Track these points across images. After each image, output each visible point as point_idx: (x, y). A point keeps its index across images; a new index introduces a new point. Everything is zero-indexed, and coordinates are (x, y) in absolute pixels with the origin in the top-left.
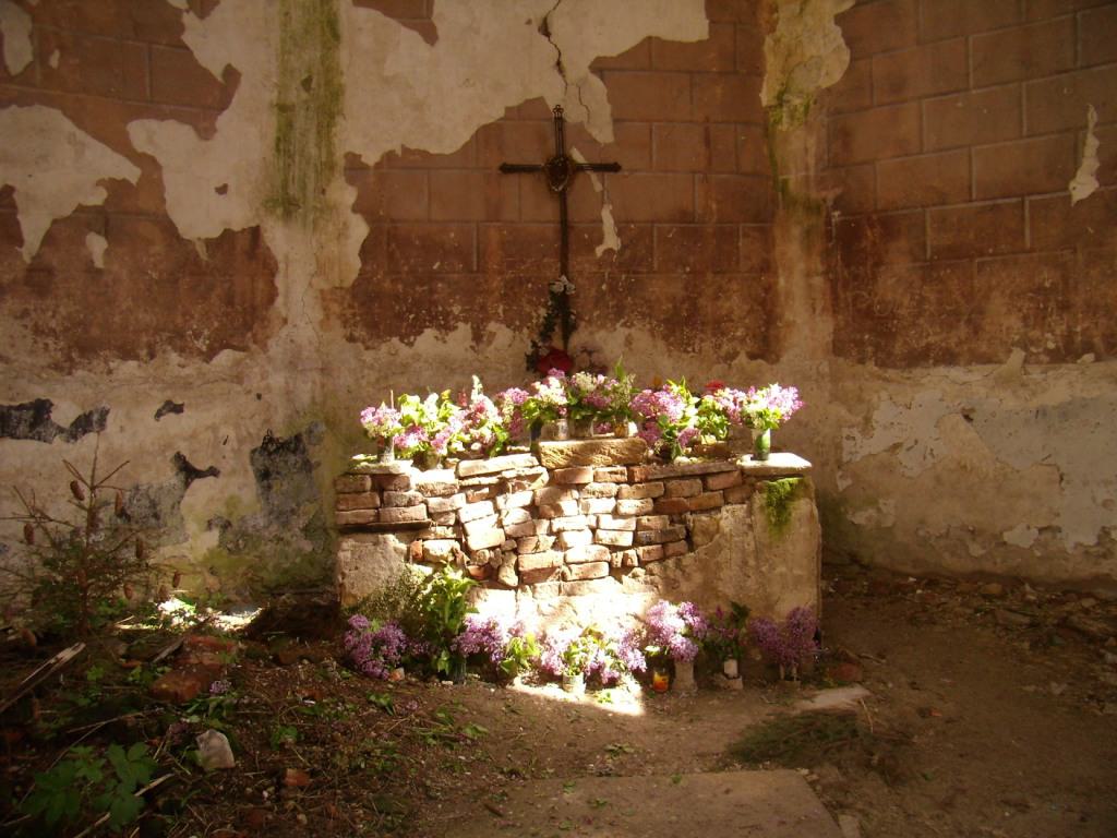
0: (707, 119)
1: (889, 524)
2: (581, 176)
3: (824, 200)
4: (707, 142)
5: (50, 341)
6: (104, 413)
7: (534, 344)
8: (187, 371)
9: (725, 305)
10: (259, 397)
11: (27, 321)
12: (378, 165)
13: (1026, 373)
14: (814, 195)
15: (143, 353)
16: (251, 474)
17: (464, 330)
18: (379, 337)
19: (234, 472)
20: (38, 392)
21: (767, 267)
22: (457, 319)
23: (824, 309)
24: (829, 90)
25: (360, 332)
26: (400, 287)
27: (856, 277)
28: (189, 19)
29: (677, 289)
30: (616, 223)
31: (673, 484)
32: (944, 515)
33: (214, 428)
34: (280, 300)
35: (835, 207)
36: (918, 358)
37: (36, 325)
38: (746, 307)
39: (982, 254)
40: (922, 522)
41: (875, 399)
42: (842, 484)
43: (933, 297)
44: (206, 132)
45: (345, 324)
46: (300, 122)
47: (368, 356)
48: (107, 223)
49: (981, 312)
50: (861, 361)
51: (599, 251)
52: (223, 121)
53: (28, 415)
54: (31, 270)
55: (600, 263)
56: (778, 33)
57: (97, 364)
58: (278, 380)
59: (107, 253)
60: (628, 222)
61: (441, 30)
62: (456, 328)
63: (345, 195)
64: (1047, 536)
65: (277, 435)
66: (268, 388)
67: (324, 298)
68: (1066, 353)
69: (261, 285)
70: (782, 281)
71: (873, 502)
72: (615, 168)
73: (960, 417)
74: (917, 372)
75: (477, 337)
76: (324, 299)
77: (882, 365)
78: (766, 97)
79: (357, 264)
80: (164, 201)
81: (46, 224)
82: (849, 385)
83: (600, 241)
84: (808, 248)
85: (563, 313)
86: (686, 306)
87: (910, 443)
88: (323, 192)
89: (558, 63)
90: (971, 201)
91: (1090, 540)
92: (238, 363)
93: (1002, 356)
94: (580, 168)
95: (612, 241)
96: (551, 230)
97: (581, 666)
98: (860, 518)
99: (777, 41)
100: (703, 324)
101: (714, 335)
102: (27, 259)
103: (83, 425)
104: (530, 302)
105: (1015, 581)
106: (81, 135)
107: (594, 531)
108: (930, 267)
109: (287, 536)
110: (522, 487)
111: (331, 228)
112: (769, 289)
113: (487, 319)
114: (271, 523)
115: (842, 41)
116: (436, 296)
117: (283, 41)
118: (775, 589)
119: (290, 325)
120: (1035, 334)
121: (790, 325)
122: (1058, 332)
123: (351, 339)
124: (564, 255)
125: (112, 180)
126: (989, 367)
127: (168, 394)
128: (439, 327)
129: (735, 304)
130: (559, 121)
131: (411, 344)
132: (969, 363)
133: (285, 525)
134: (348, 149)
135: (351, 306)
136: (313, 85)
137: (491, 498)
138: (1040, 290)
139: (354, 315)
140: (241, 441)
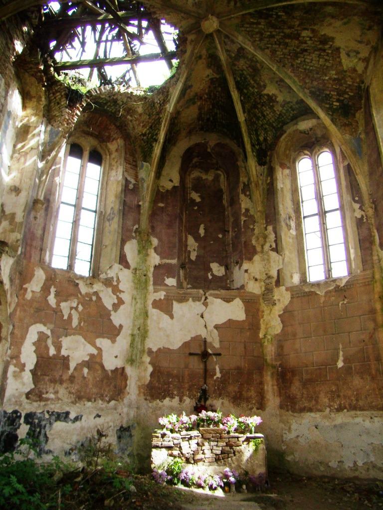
0: (245, 341)
1: (297, 460)
2: (210, 357)
3: (277, 365)
4: (245, 348)
5: (72, 395)
6: (82, 416)
7: (196, 403)
9: (250, 394)
10: (120, 414)
11: (68, 390)
12: (156, 352)
13: (331, 415)
14: (274, 363)
15: (93, 400)
16: (116, 437)
17: (177, 398)
18: (154, 399)
19: (112, 436)
20: (67, 409)
21: (261, 383)
22: (175, 395)
23: (277, 396)
24: (277, 334)
26: (160, 386)
27: (285, 386)
28: (112, 313)
29: (236, 389)
30: (220, 370)
31: (230, 439)
32: (313, 457)
33: (108, 423)
34: (128, 387)
35: (279, 367)
36: (303, 410)
37: (69, 391)
38: (256, 394)
39: (317, 381)
40: (306, 460)
41: (291, 421)
42: (284, 448)
44: (114, 341)
45: (144, 395)
46: (137, 339)
47: (150, 405)
48: (88, 365)
49: (318, 397)
50: (288, 411)
51: (215, 378)
52: (118, 338)
53: (64, 415)
55: (215, 381)
56: (264, 318)
57: (82, 403)
58: (125, 410)
59: (88, 373)
60: (223, 370)
61: (175, 315)
62: (174, 398)
63: (147, 359)
64: (340, 464)
65: (124, 426)
66: (123, 412)
67: (139, 387)
68: (340, 409)
69: (123, 383)
70: (266, 387)
71: (293, 454)
72: (220, 355)
73: (314, 427)
74: (302, 414)
75: (181, 401)
76: (139, 388)
77: (293, 412)
78: (261, 335)
79: (149, 378)
80: (102, 359)
81: (75, 365)
82: (285, 418)
83: (215, 375)
84: (272, 376)
85: (204, 395)
86: (238, 394)
88: (141, 358)
89: (205, 325)
90: (313, 366)
91: (351, 465)
92: (115, 405)
93: (155, 397)
94: (211, 354)
95: (218, 375)
96: (202, 371)
97: (208, 484)
98: (289, 458)
99: (264, 320)
100: (244, 399)
101: (247, 402)
102: (70, 374)
103: (77, 419)
104: (196, 391)
105: (332, 478)
106: (85, 342)
107: (212, 450)
108: (305, 384)
109: (123, 456)
110: (195, 439)
111: (142, 368)
112: (262, 389)
114: (120, 452)
115: (280, 322)
116: (170, 389)
117: (134, 317)
118: (255, 467)
119: (130, 395)
120: (332, 404)
122: (337, 403)
123: (146, 399)
124: (205, 378)
125: (91, 354)
126: (321, 413)
127: (98, 412)
128: (170, 397)
129: (252, 393)
130: (205, 341)
131: (162, 402)
132: (316, 412)
133: (123, 453)
134: (148, 347)
135: (147, 390)
136: (141, 329)
137: (188, 441)
138: (332, 391)
139: (147, 392)
140: (114, 427)
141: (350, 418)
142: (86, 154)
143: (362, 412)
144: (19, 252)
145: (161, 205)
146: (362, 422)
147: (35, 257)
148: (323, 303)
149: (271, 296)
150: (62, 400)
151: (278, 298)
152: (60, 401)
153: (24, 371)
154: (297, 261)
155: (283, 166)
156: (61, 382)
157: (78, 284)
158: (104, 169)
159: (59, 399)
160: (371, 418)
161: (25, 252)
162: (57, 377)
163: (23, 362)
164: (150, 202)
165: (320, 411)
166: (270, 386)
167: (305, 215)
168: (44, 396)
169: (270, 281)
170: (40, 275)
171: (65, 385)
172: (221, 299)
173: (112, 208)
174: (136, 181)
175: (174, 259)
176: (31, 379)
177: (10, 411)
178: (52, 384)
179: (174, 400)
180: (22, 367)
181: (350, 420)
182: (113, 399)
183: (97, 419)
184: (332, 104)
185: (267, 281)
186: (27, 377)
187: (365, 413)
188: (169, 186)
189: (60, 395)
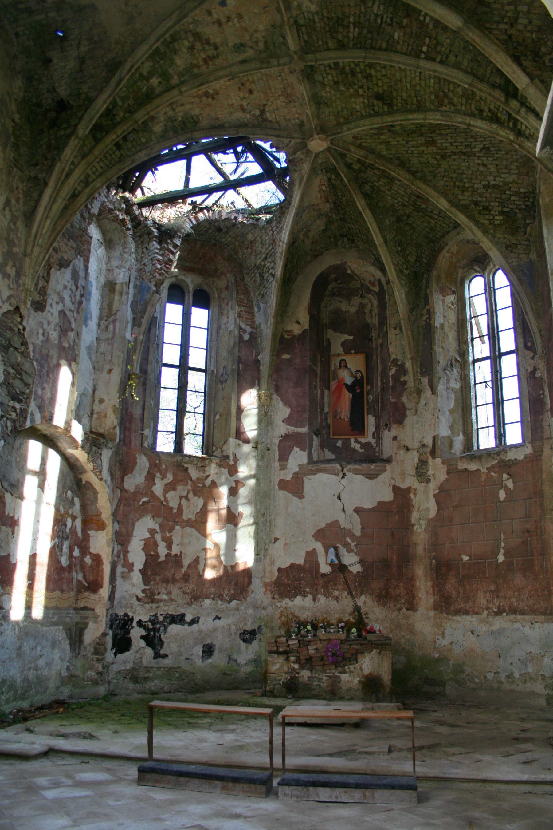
6: (199, 618)
8: (223, 607)
17: (310, 597)
20: (182, 611)
22: (308, 593)
25: (277, 596)
36: (458, 612)
43: (462, 591)
45: (272, 592)
47: (279, 604)
50: (442, 612)
53: (180, 617)
54: (184, 575)
68: (499, 613)
70: (417, 583)
73: (470, 633)
75: (314, 600)
77: (447, 614)
87: (456, 642)
92: (238, 605)
102: (183, 572)
103: (195, 621)
113: (318, 594)
121: (420, 599)
126: (478, 616)
127: (217, 614)
128: (302, 596)
129: (401, 591)
140: (237, 630)
141: (509, 623)
142: (189, 298)
143: (523, 616)
144: (117, 440)
145: (286, 356)
146: (521, 628)
147: (135, 442)
148: (485, 481)
149: (424, 471)
150: (176, 601)
151: (433, 472)
152: (174, 603)
153: (133, 571)
154: (461, 423)
155: (444, 292)
156: (174, 581)
157: (187, 469)
158: (213, 312)
159: (172, 600)
160: (532, 624)
161: (124, 438)
162: (170, 576)
163: (131, 561)
164: (272, 355)
165: (477, 613)
166: (422, 582)
167: (475, 358)
168: (156, 597)
169: (424, 450)
170: (143, 462)
171: (178, 585)
172: (363, 475)
173: (225, 367)
174: (252, 328)
175: (304, 426)
176: (141, 579)
177: (121, 614)
178: (164, 584)
179: (307, 599)
180: (130, 567)
181: (508, 625)
182: (235, 599)
183: (217, 621)
184: (494, 219)
185: (421, 451)
186: (136, 577)
187: (526, 617)
188: (297, 330)
189: (173, 596)
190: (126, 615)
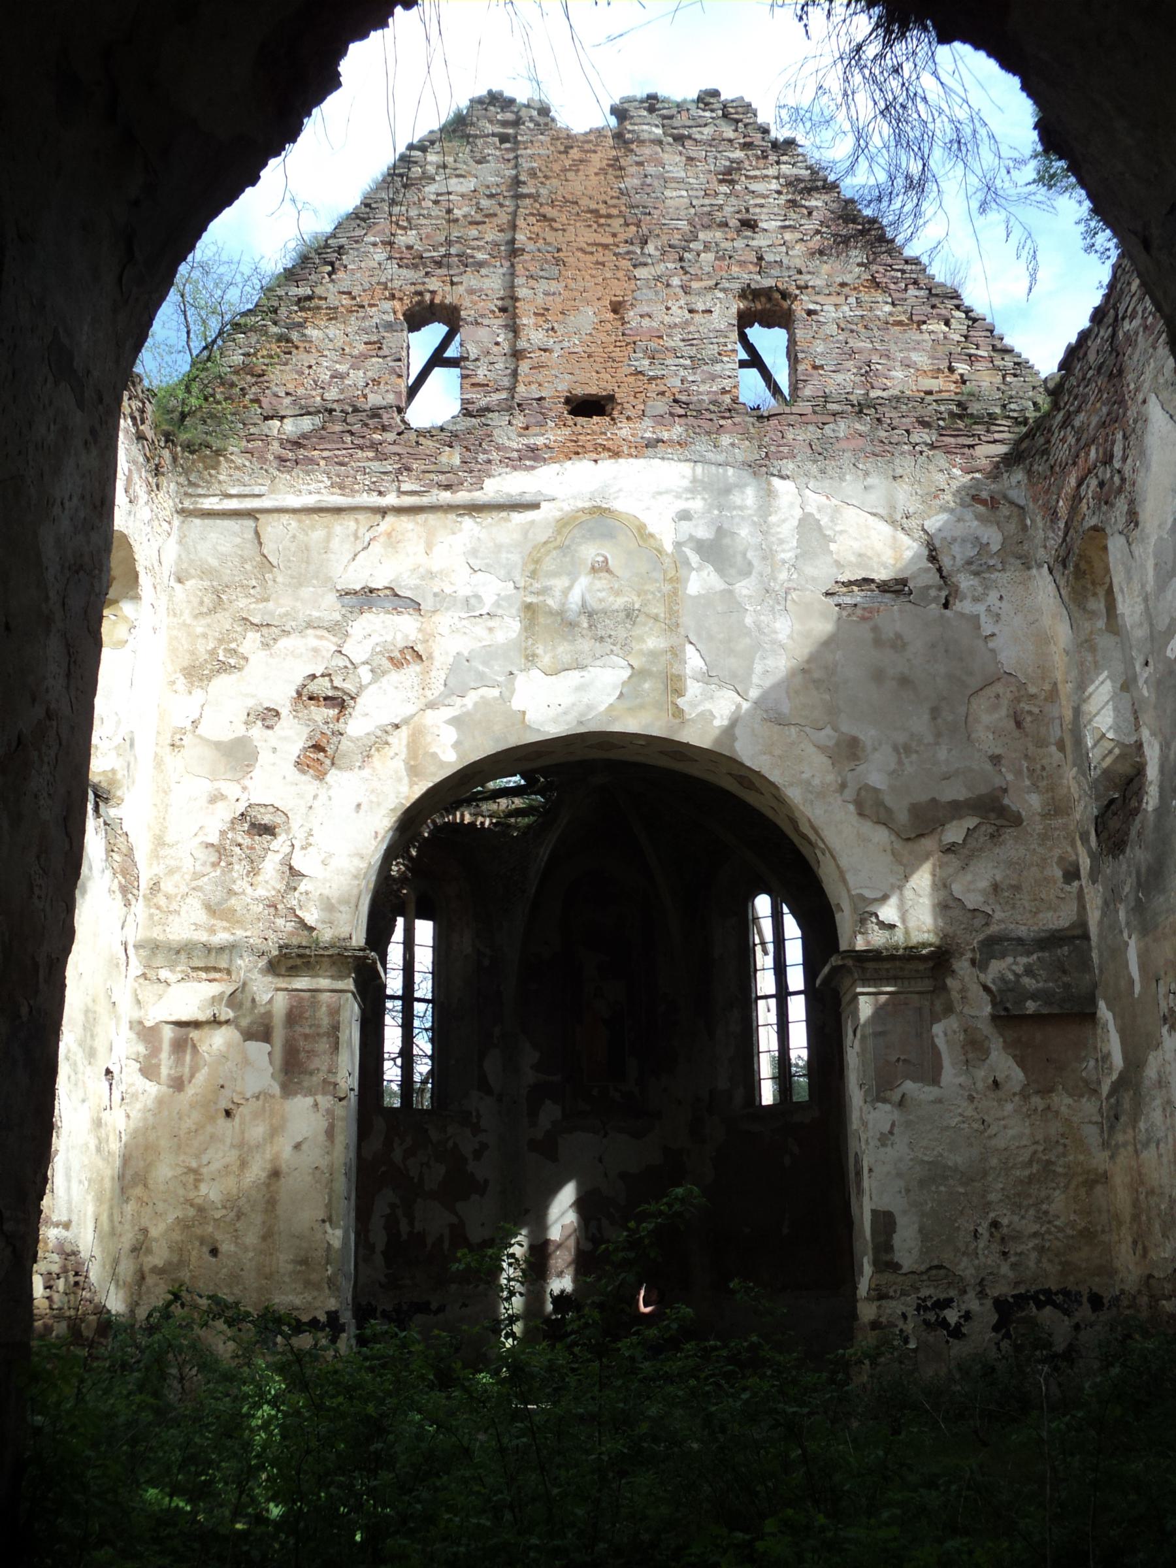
190: (369, 1304)
